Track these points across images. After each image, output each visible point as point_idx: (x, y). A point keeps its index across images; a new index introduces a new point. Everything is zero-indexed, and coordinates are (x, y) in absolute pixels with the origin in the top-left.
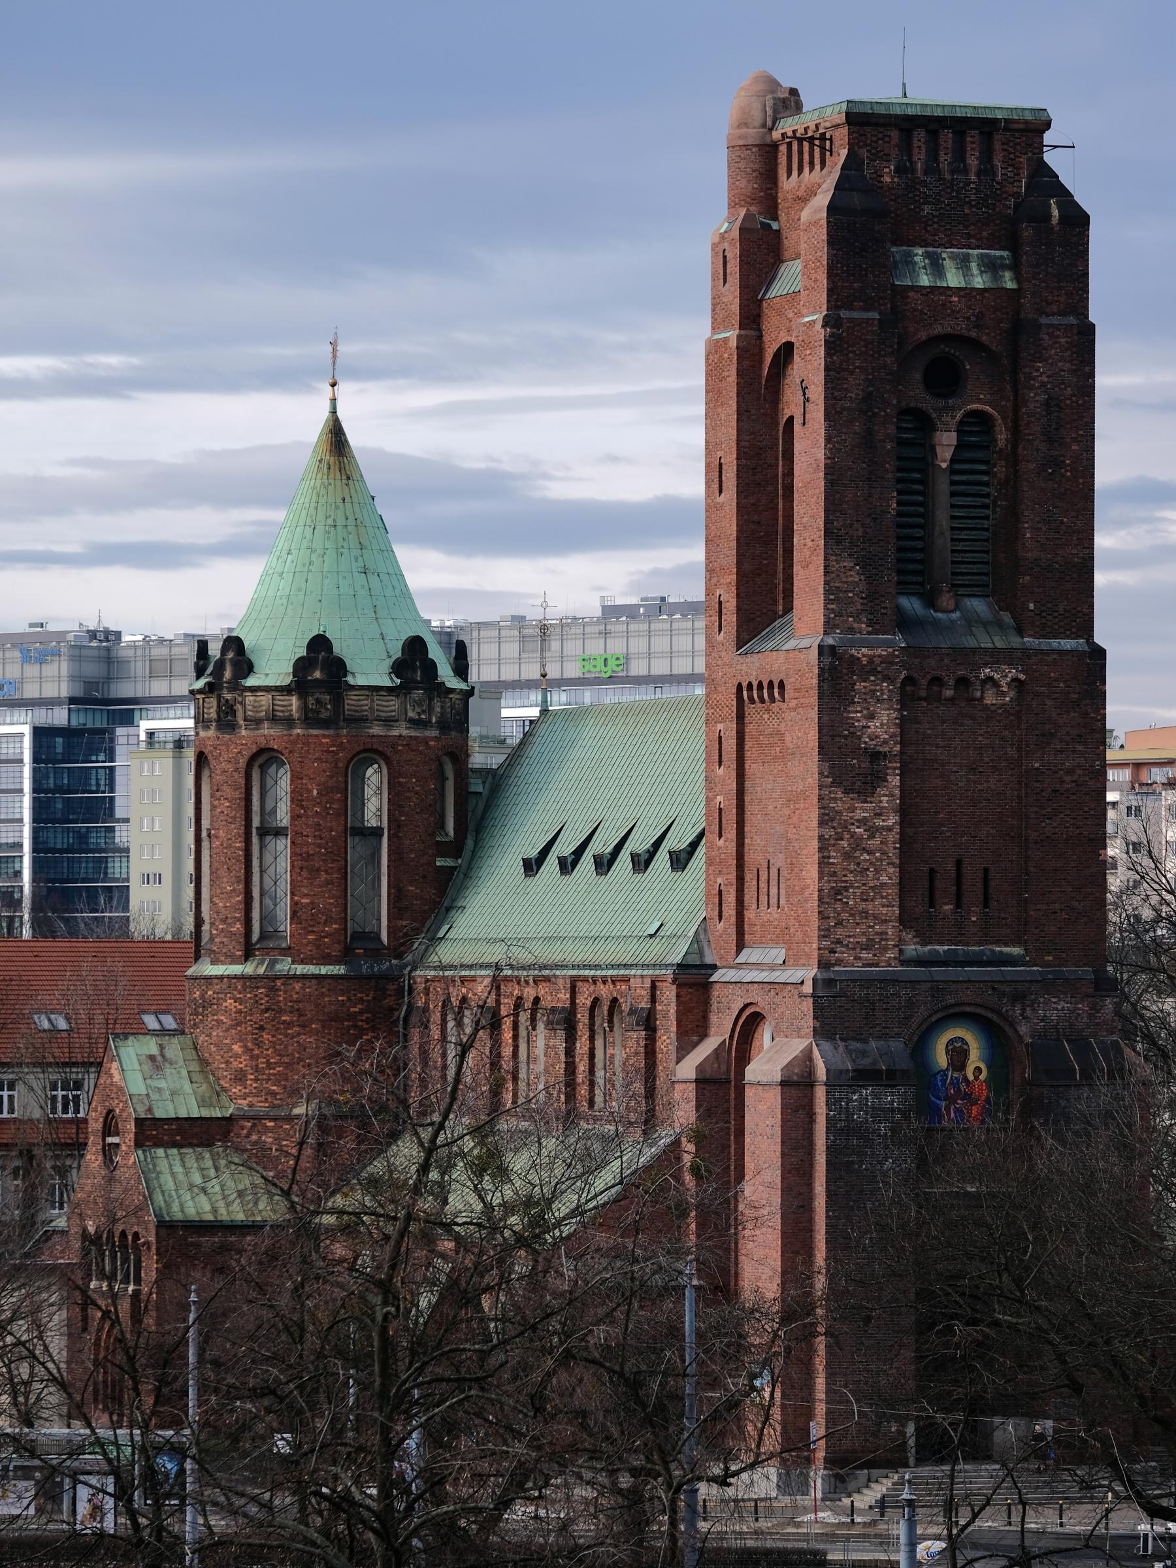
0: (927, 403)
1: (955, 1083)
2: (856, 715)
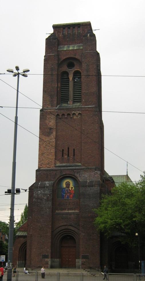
0: (68, 70)
1: (67, 190)
2: (47, 122)
